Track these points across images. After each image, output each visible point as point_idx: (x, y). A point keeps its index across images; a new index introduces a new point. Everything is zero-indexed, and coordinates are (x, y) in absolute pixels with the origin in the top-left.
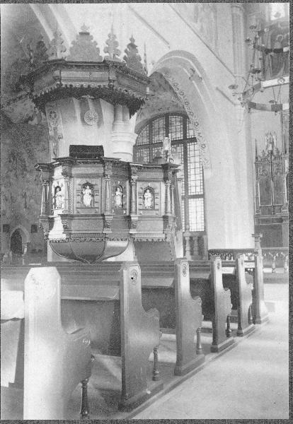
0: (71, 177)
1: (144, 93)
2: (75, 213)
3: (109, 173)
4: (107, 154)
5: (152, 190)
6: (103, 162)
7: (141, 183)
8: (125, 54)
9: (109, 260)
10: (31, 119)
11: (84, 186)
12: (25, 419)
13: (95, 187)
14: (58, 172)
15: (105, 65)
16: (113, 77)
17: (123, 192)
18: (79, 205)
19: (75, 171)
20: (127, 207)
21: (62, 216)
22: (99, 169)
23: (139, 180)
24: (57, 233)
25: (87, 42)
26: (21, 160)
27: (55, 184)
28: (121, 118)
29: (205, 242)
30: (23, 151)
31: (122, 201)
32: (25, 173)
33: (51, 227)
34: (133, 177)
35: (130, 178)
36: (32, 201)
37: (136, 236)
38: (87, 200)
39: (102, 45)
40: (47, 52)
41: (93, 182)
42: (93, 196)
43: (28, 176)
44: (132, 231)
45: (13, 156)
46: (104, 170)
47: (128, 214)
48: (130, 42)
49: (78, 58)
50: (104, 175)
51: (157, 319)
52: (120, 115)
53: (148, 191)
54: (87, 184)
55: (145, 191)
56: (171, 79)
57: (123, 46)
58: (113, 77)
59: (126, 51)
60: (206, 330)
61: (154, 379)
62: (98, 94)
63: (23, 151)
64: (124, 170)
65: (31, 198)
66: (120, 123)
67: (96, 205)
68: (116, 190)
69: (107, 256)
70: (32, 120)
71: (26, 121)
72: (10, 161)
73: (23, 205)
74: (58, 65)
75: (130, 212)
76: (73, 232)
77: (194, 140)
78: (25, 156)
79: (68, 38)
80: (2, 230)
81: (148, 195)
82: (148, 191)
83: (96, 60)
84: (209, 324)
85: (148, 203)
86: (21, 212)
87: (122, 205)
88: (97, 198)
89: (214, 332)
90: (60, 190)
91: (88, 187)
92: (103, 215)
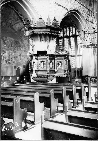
0: (38, 59)
1: (58, 33)
2: (39, 70)
3: (48, 58)
4: (48, 53)
5: (61, 62)
6: (47, 55)
7: (58, 60)
8: (53, 23)
9: (49, 82)
10: (22, 29)
11: (41, 62)
12: (69, 57)
13: (44, 62)
14: (34, 57)
15: (47, 28)
16: (49, 30)
17: (53, 63)
18: (40, 67)
19: (39, 58)
20: (54, 67)
21: (36, 71)
22: (46, 57)
23: (57, 59)
24: (34, 75)
25: (41, 21)
26: (19, 43)
27: (33, 61)
28: (52, 39)
29: (82, 71)
30: (19, 40)
31: (52, 66)
32: (20, 48)
33: (32, 73)
34: (55, 58)
35: (54, 59)
36: (23, 57)
37: (57, 76)
38: (42, 66)
39: (46, 22)
40: (31, 24)
41: (44, 60)
42: (44, 64)
43: (21, 49)
44: (55, 74)
45: (16, 42)
46: (47, 57)
47: (54, 69)
48: (54, 19)
49: (39, 26)
50: (47, 59)
51: (58, 101)
52: (52, 38)
53: (60, 62)
54: (42, 61)
55: (59, 62)
56: (69, 18)
57: (52, 21)
58: (49, 30)
59: (53, 22)
60: (72, 102)
61: (57, 113)
62: (45, 35)
63: (19, 40)
64: (52, 57)
65: (22, 56)
66: (51, 41)
67: (45, 67)
68: (51, 63)
69: (48, 81)
70: (22, 29)
71: (20, 30)
72: (15, 44)
73: (20, 59)
74: (37, 55)
75: (54, 69)
76: (38, 75)
77: (78, 36)
78: (20, 42)
79: (37, 19)
80: (14, 68)
81: (60, 63)
82: (60, 62)
83: (44, 26)
84: (72, 101)
85: (60, 66)
86: (20, 61)
87: (52, 67)
88: (45, 65)
89: (73, 103)
90: (35, 63)
91: (42, 62)
92: (47, 70)
